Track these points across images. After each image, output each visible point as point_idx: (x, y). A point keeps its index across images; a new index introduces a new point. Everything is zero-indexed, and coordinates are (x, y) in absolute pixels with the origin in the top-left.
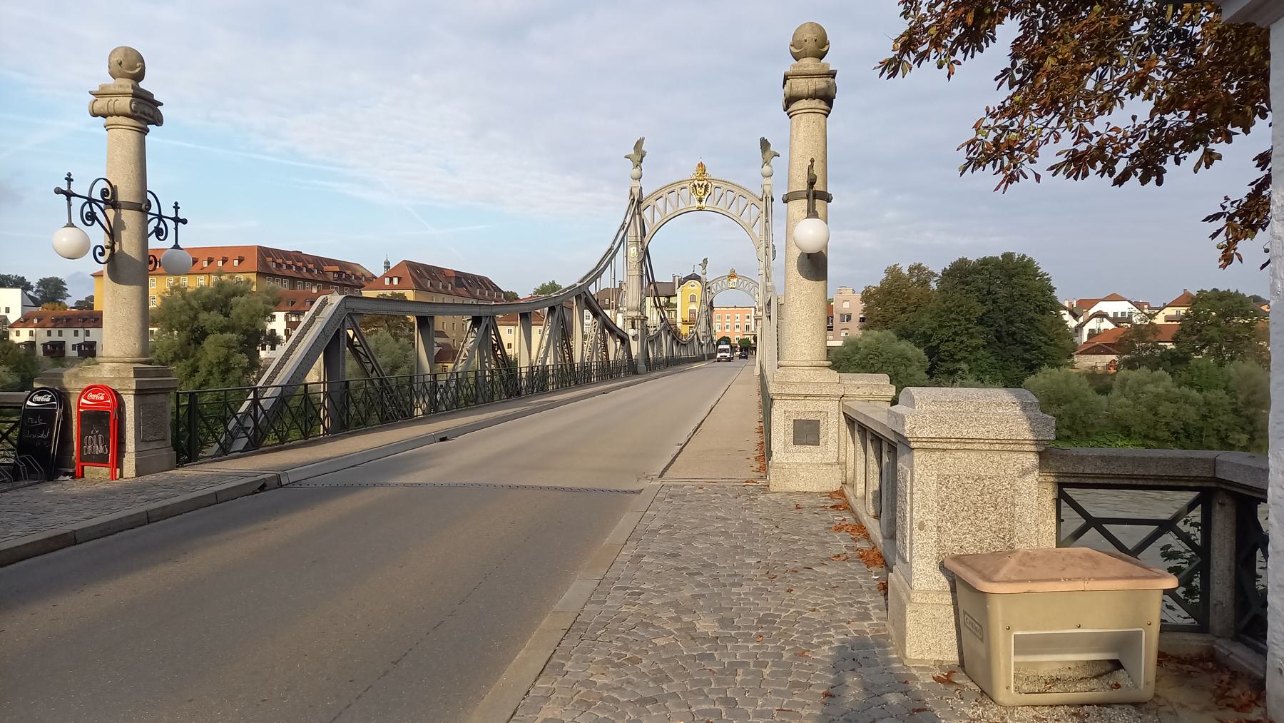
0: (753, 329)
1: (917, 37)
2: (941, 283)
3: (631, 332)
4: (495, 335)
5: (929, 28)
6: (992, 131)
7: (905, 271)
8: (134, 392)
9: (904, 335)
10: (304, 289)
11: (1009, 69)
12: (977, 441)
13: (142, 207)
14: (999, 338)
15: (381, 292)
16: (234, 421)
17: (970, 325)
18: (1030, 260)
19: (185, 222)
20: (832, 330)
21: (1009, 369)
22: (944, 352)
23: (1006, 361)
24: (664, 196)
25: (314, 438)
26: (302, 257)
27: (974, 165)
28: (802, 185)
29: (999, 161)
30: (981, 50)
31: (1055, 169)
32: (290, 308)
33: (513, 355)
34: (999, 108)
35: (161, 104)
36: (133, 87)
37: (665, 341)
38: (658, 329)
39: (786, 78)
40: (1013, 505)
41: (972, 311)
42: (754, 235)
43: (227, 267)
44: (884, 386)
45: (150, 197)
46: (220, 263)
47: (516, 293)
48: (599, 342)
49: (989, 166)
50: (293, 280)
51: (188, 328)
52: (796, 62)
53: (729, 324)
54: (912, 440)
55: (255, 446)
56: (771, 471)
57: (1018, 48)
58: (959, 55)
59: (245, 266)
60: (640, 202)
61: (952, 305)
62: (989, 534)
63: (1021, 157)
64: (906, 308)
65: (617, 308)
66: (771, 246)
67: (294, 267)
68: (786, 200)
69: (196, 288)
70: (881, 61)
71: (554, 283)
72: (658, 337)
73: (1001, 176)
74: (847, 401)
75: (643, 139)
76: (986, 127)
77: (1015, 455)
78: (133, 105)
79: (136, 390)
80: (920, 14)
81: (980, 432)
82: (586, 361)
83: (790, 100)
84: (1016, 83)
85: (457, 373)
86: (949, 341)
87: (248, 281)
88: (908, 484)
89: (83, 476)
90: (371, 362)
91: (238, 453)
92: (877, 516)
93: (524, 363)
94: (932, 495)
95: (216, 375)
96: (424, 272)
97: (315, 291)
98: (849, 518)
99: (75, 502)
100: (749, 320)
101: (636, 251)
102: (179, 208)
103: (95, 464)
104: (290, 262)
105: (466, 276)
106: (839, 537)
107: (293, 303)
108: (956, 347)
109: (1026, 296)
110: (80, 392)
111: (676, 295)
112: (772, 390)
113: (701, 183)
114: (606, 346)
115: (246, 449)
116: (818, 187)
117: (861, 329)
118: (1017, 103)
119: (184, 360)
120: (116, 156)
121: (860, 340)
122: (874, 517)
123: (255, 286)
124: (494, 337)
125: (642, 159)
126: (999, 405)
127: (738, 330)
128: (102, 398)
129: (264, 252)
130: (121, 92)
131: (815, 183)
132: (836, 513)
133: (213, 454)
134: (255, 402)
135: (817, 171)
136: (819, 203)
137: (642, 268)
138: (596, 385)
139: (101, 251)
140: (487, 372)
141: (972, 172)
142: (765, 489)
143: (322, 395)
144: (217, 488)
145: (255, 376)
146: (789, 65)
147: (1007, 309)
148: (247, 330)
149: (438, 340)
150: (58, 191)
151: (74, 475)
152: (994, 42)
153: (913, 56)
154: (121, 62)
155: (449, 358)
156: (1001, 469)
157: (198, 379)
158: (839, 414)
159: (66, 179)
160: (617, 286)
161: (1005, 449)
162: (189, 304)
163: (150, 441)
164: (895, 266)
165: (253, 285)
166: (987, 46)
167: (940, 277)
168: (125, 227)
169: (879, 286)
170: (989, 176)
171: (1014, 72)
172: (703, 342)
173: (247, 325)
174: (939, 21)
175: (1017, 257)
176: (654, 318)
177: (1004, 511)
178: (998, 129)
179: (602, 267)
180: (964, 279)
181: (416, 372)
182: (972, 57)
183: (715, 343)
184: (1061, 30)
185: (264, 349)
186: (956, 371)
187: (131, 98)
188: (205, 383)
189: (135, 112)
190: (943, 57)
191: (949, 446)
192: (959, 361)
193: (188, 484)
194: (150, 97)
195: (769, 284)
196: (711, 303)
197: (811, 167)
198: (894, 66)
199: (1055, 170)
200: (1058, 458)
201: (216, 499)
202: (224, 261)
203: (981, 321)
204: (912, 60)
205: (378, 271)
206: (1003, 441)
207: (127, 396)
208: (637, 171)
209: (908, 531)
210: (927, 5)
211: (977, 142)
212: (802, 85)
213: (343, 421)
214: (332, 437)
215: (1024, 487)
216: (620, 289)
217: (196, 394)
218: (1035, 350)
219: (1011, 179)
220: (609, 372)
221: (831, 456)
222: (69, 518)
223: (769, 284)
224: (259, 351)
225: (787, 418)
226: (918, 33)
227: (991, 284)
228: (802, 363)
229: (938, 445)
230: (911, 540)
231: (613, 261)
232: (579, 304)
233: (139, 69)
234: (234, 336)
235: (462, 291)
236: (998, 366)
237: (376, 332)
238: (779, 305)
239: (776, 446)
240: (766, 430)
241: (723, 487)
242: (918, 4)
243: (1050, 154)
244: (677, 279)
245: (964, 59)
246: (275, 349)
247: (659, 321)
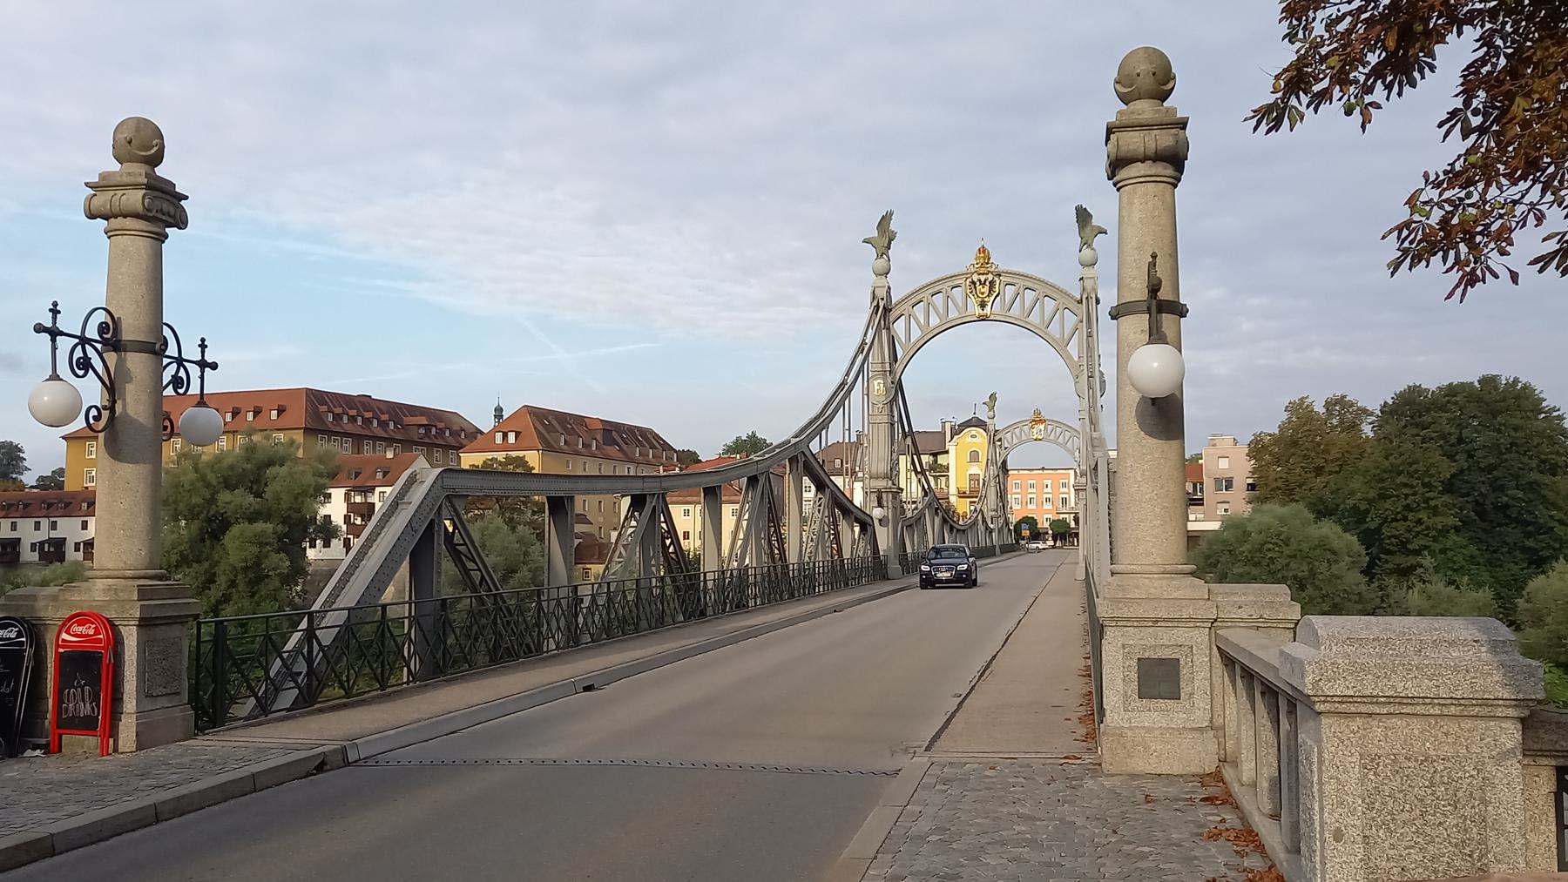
0: (1073, 505)
1: (1310, 70)
2: (1380, 426)
3: (877, 513)
4: (665, 522)
5: (1327, 56)
6: (1436, 207)
7: (1319, 408)
8: (137, 623)
9: (1322, 511)
10: (374, 452)
11: (1461, 110)
12: (1421, 701)
13: (155, 348)
14: (1481, 514)
15: (490, 455)
16: (278, 662)
17: (1431, 494)
18: (1526, 387)
19: (214, 366)
20: (1202, 504)
21: (1501, 566)
22: (1390, 538)
23: (1495, 552)
24: (925, 299)
25: (395, 688)
26: (372, 403)
27: (1412, 259)
28: (1139, 292)
29: (1452, 253)
30: (1413, 84)
31: (1543, 262)
32: (352, 483)
33: (692, 549)
34: (1446, 173)
35: (186, 198)
36: (147, 175)
37: (932, 526)
38: (920, 506)
39: (1110, 131)
40: (1484, 802)
41: (1432, 471)
42: (1070, 357)
43: (261, 422)
44: (1282, 604)
45: (167, 332)
46: (250, 416)
47: (695, 453)
48: (826, 529)
49: (1436, 260)
50: (358, 439)
51: (202, 516)
52: (1125, 107)
53: (1034, 496)
54: (1317, 699)
55: (307, 701)
56: (1104, 740)
57: (1471, 80)
58: (1379, 94)
59: (288, 419)
60: (887, 310)
61: (1399, 461)
62: (1446, 848)
63: (1486, 246)
64: (1323, 467)
65: (854, 472)
66: (1097, 374)
67: (360, 419)
68: (1115, 315)
69: (214, 454)
70: (1254, 108)
71: (754, 435)
72: (919, 519)
73: (1455, 276)
74: (1222, 628)
75: (891, 214)
76: (1425, 203)
77: (1482, 724)
78: (146, 201)
79: (141, 619)
80: (1313, 36)
81: (1425, 687)
82: (807, 559)
83: (1116, 165)
84: (1473, 130)
85: (609, 584)
86: (1397, 521)
87: (292, 442)
88: (1315, 768)
89: (60, 751)
90: (479, 570)
91: (284, 713)
92: (1276, 816)
93: (709, 566)
94: (1352, 785)
95: (241, 587)
96: (554, 423)
97: (390, 455)
98: (1231, 818)
99: (50, 790)
100: (1066, 490)
101: (882, 386)
102: (206, 346)
103: (73, 731)
104: (353, 412)
105: (618, 427)
106: (1214, 850)
107: (357, 474)
108: (1409, 531)
109: (1522, 445)
110: (60, 623)
111: (947, 452)
112: (1102, 611)
113: (983, 278)
114: (837, 535)
115: (295, 705)
116: (1164, 294)
117: (1249, 502)
118: (1473, 166)
119: (195, 565)
120: (121, 274)
121: (1250, 520)
122: (1271, 817)
123: (301, 451)
124: (664, 525)
125: (889, 243)
126: (1452, 644)
127: (1048, 506)
128: (91, 632)
129: (316, 398)
130: (129, 182)
131: (1159, 290)
132: (1210, 809)
133: (247, 715)
134: (310, 635)
135: (1162, 271)
136: (1166, 318)
137: (892, 411)
138: (821, 598)
139: (96, 414)
140: (654, 580)
141: (1410, 269)
142: (1096, 769)
143: (406, 621)
144: (255, 768)
145: (299, 588)
146: (1112, 109)
147: (1492, 468)
148: (289, 517)
149: (578, 528)
150: (39, 329)
151: (48, 750)
152: (1434, 72)
153: (1305, 99)
154: (131, 141)
155: (594, 555)
156: (1461, 744)
157: (215, 593)
158: (1211, 649)
159: (50, 310)
160: (854, 439)
161: (1466, 713)
162: (203, 478)
163: (158, 696)
164: (1302, 399)
165: (298, 448)
166: (1423, 78)
167: (1378, 416)
168: (132, 378)
169: (1277, 432)
170: (1437, 274)
171: (1469, 114)
172: (992, 526)
173: (289, 509)
174: (1344, 47)
175: (1504, 382)
176: (911, 488)
177: (1468, 812)
178: (1446, 205)
179: (829, 412)
180: (1418, 420)
181: (546, 582)
182: (1400, 94)
183: (1011, 528)
184: (1539, 53)
185: (313, 546)
186: (1412, 568)
187: (144, 191)
188: (226, 599)
189: (149, 210)
190: (1352, 97)
191: (1377, 709)
192: (1418, 552)
193: (213, 761)
194: (168, 188)
195: (1095, 435)
196: (1004, 463)
197: (1153, 265)
198: (1275, 114)
199: (1542, 263)
200: (1554, 727)
201: (253, 785)
202: (257, 412)
203: (1449, 487)
204: (1304, 104)
205: (486, 423)
206: (1462, 702)
207: (127, 628)
208: (882, 262)
209: (1318, 843)
210: (1324, 22)
211: (1414, 225)
212: (1133, 141)
213: (437, 663)
214: (421, 686)
215: (1499, 774)
216: (859, 443)
217: (225, 623)
218: (1544, 533)
219: (1471, 280)
220: (841, 576)
221: (1201, 717)
222: (44, 815)
223: (1095, 435)
224: (305, 548)
225: (1127, 656)
226: (1312, 65)
227: (1464, 428)
228: (1148, 569)
229: (1353, 708)
230: (1323, 857)
231: (847, 402)
232: (795, 470)
233: (156, 149)
234: (269, 527)
235: (613, 450)
236: (1481, 561)
237: (482, 516)
238: (1111, 474)
239: (1111, 700)
240: (1094, 672)
241: (1029, 766)
242: (1310, 20)
243: (1529, 242)
244: (948, 426)
245: (1388, 99)
246: (329, 546)
247: (921, 493)
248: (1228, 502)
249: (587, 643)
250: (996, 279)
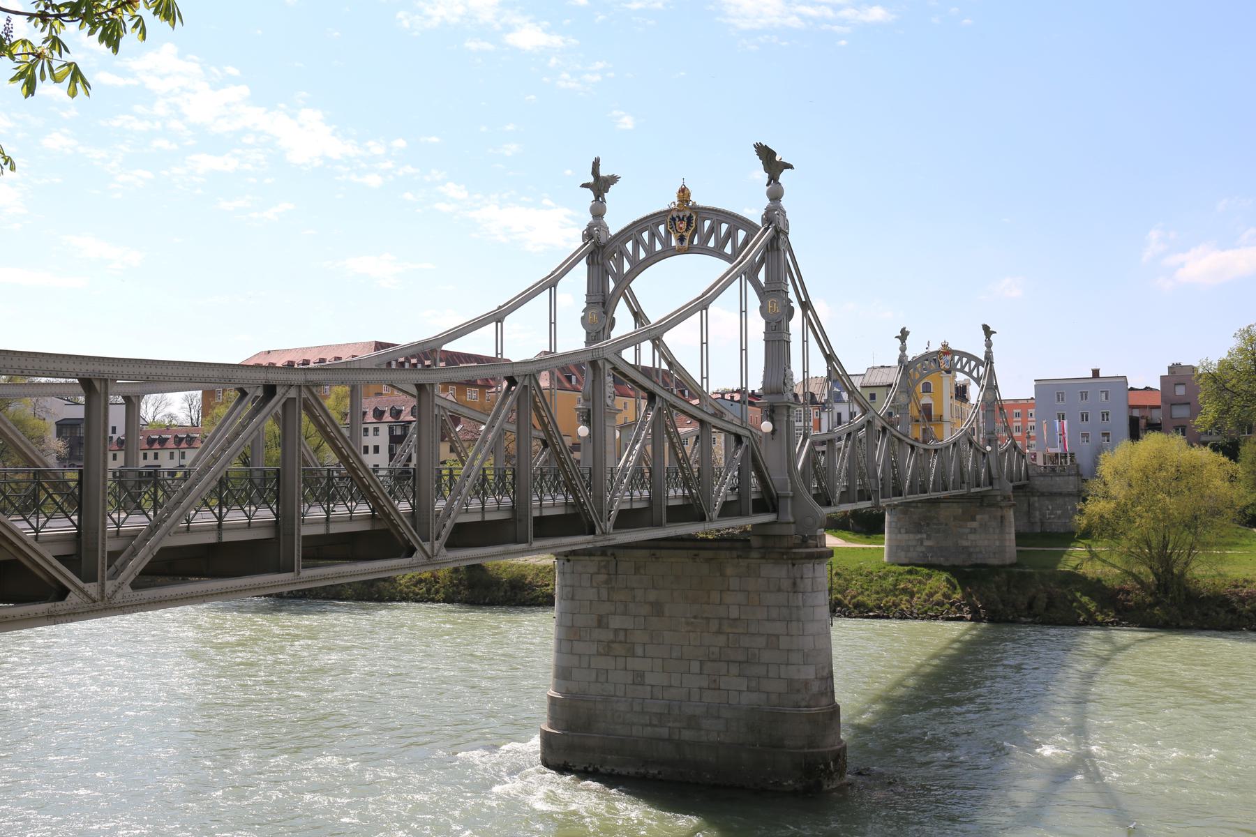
248: (1189, 404)
250: (693, 215)
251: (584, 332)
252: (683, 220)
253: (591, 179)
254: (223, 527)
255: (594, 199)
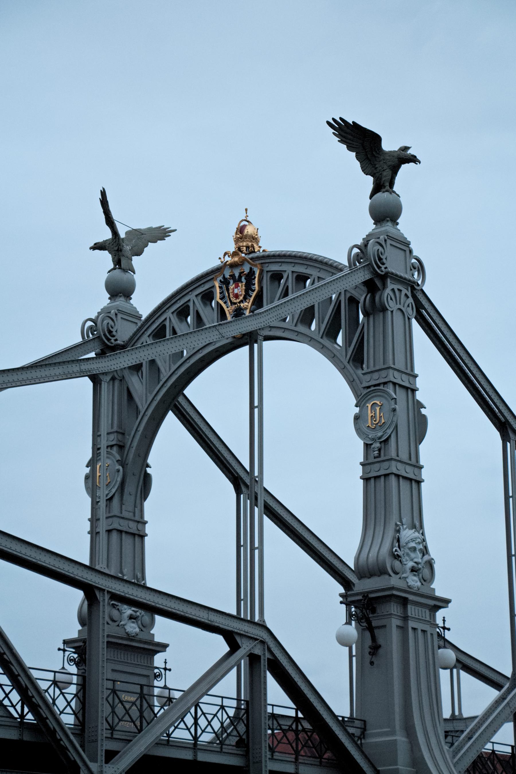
19: (170, 670)
249: (266, 766)
251: (360, 444)
252: (240, 280)
253: (107, 235)
254: (198, 747)
255: (112, 266)
